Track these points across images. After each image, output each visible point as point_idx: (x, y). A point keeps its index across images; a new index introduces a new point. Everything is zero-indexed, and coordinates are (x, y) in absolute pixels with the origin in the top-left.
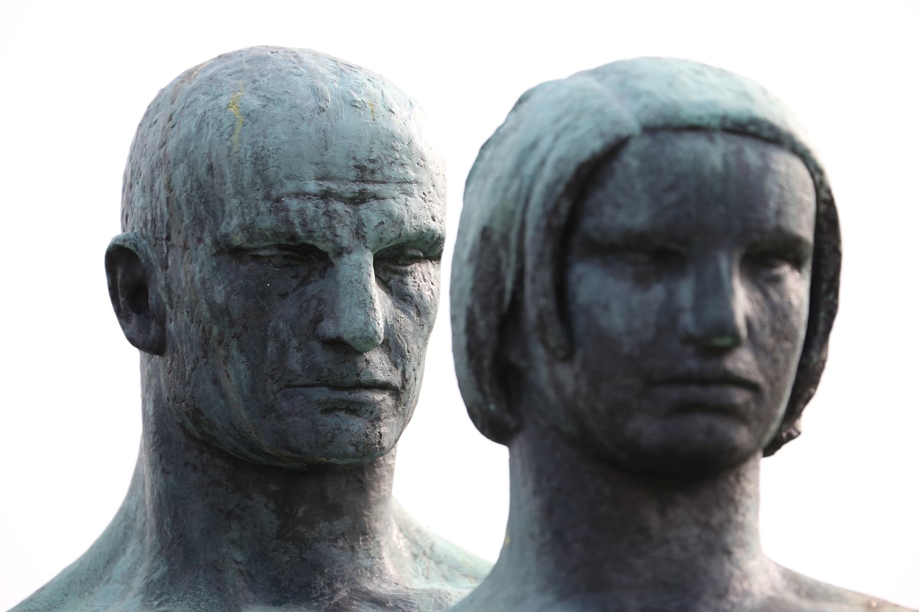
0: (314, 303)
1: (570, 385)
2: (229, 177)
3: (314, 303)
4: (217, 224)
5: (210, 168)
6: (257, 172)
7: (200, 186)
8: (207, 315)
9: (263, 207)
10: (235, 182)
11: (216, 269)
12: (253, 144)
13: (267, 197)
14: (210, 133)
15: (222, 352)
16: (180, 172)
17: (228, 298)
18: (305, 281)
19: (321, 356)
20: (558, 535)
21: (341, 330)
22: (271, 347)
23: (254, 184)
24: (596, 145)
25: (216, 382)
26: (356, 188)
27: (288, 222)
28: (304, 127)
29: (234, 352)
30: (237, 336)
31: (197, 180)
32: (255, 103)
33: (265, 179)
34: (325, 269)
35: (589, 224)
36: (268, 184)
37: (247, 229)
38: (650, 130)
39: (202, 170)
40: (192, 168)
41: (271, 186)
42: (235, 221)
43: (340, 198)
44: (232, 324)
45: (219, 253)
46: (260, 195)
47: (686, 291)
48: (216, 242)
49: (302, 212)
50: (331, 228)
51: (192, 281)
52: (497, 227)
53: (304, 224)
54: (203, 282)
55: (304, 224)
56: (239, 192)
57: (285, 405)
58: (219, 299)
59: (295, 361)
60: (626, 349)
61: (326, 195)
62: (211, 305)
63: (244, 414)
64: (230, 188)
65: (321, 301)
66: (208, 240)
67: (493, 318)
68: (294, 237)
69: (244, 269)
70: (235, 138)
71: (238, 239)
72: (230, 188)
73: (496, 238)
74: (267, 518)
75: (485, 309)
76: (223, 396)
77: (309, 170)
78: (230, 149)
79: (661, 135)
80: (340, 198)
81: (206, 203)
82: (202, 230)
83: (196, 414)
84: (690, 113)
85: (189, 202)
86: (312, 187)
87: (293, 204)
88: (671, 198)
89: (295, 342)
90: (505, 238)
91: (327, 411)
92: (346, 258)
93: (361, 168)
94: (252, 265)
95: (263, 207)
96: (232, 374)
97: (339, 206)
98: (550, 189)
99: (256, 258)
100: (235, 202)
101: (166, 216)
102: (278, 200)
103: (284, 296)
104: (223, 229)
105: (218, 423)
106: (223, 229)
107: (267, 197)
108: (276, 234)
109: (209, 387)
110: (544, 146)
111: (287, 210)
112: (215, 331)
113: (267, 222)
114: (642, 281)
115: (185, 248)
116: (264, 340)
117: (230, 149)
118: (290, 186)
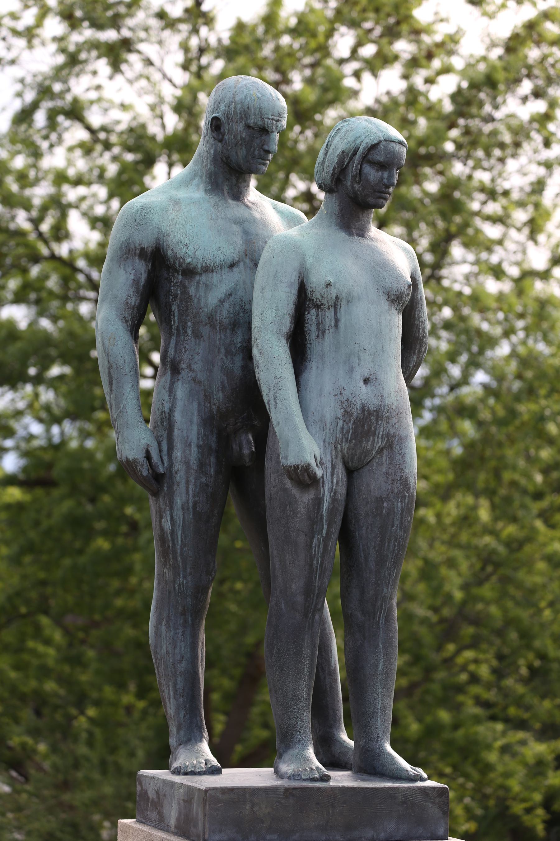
0: (263, 141)
1: (357, 188)
2: (253, 111)
3: (263, 141)
4: (247, 120)
5: (248, 108)
6: (259, 111)
7: (244, 111)
8: (239, 139)
9: (260, 119)
10: (254, 113)
11: (244, 129)
12: (260, 105)
13: (261, 117)
14: (248, 99)
15: (240, 147)
16: (239, 106)
17: (246, 136)
18: (261, 136)
19: (262, 153)
20: (342, 215)
21: (270, 149)
22: (252, 149)
23: (258, 114)
24: (376, 142)
25: (236, 153)
26: (278, 118)
27: (264, 124)
28: (270, 103)
29: (244, 148)
30: (245, 145)
31: (244, 109)
32: (260, 95)
33: (261, 113)
34: (266, 134)
35: (370, 157)
36: (261, 115)
37: (255, 123)
38: (385, 140)
39: (246, 108)
40: (243, 106)
41: (262, 115)
42: (252, 121)
43: (275, 120)
44: (245, 142)
45: (245, 126)
46: (259, 117)
47: (386, 175)
48: (245, 124)
49: (268, 122)
50: (272, 126)
51: (237, 130)
52: (347, 151)
53: (267, 125)
54: (240, 131)
55: (267, 125)
56: (255, 115)
57: (252, 161)
58: (244, 136)
59: (256, 153)
60: (372, 184)
61: (272, 119)
62: (241, 137)
63: (242, 161)
64: (253, 113)
65: (265, 141)
66: (244, 123)
67: (340, 169)
68: (264, 127)
69: (250, 130)
70: (255, 102)
71: (252, 125)
72: (253, 113)
73: (345, 153)
74: (234, 181)
75: (338, 167)
76: (237, 156)
77: (270, 113)
78: (254, 105)
79: (388, 142)
80: (275, 120)
81: (245, 115)
82: (243, 120)
83: (228, 158)
84: (394, 139)
85: (240, 113)
86: (270, 117)
87: (266, 120)
88: (389, 156)
89: (257, 149)
90: (348, 154)
91: (259, 164)
92: (273, 133)
93: (279, 114)
94: (252, 130)
95: (260, 119)
96: (241, 152)
97: (274, 122)
98: (364, 148)
99: (253, 129)
100: (253, 117)
101: (233, 114)
102: (263, 119)
103: (257, 138)
104: (248, 121)
105: (233, 161)
106: (248, 121)
107: (261, 117)
108: (261, 126)
109: (234, 153)
110: (363, 137)
111: (265, 121)
112: (240, 142)
113: (260, 123)
114: (378, 171)
115: (237, 122)
116: (251, 147)
117: (254, 105)
118: (266, 116)
